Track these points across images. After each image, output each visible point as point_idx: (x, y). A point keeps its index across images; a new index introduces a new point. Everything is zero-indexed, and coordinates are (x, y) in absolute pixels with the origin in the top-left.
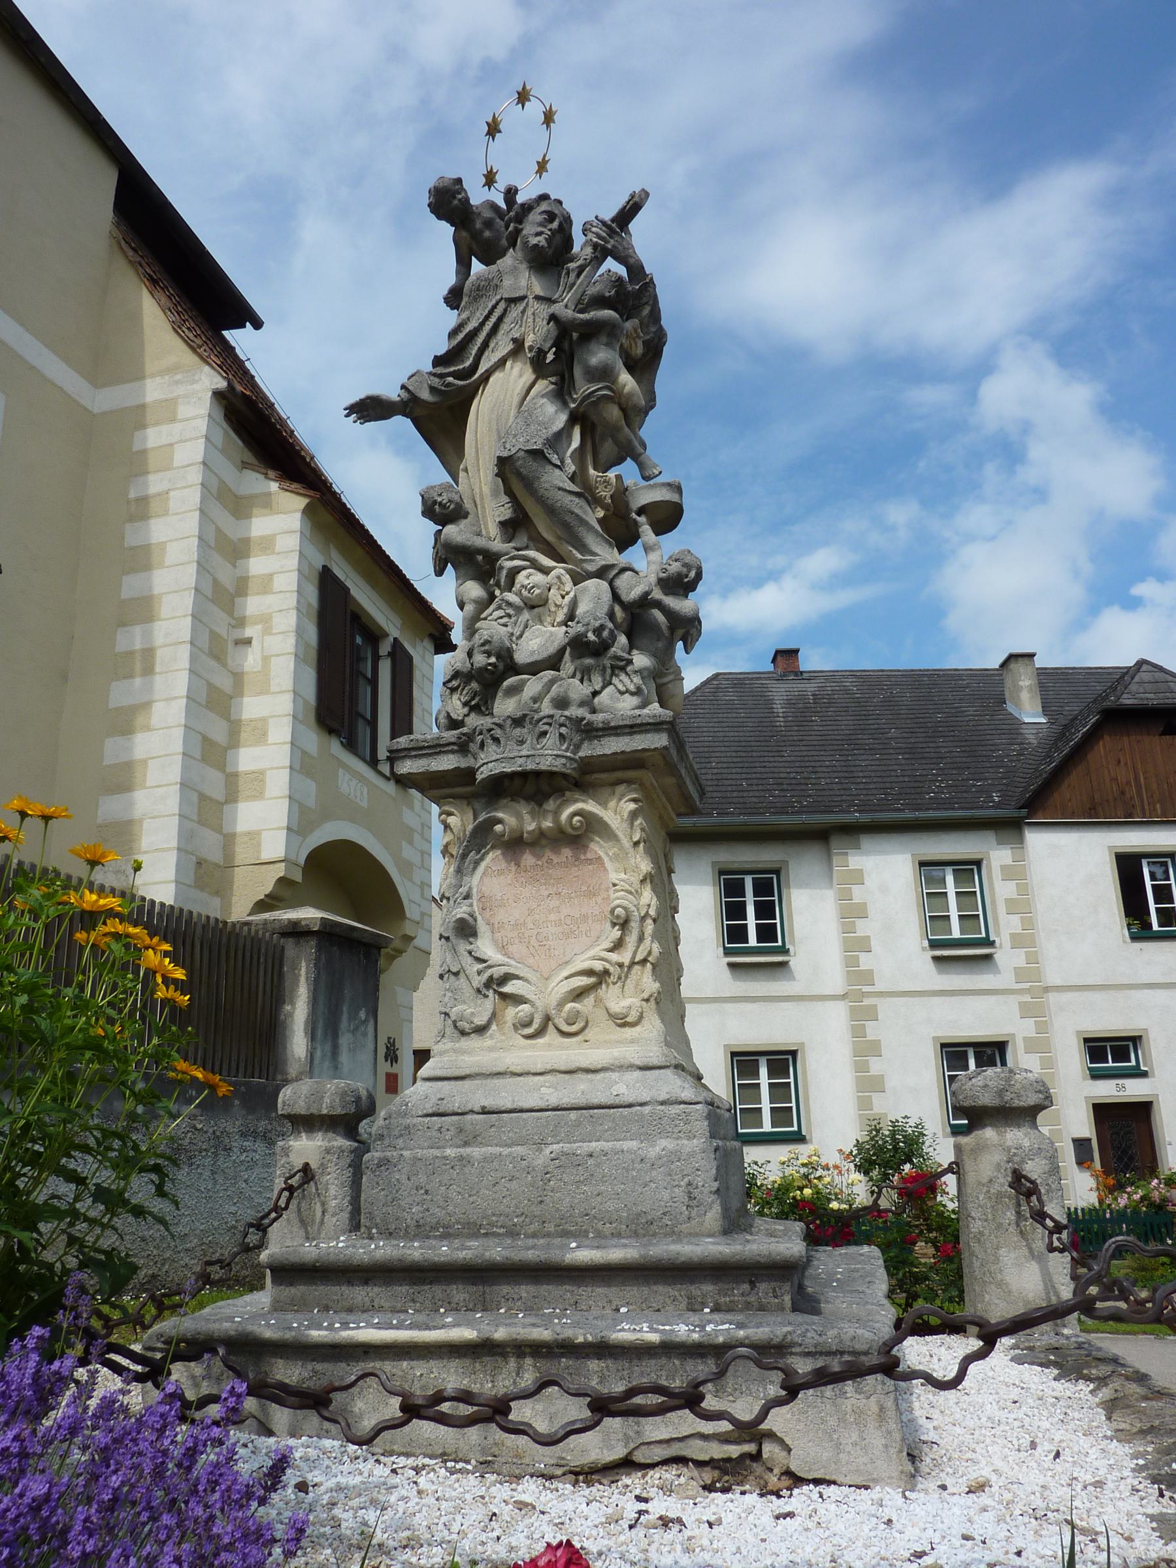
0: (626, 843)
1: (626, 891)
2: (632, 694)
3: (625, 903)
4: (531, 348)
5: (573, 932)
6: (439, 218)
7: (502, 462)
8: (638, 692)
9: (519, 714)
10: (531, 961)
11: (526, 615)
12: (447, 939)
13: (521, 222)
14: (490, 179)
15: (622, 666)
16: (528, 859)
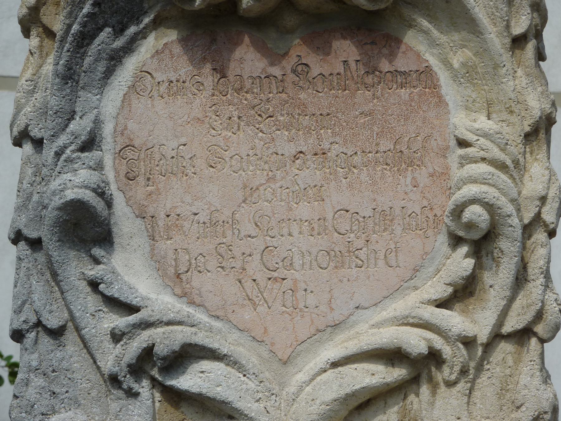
0: (496, 41)
1: (493, 163)
3: (491, 194)
5: (353, 252)
6: (19, 23)
10: (247, 315)
12: (36, 244)
16: (247, 59)
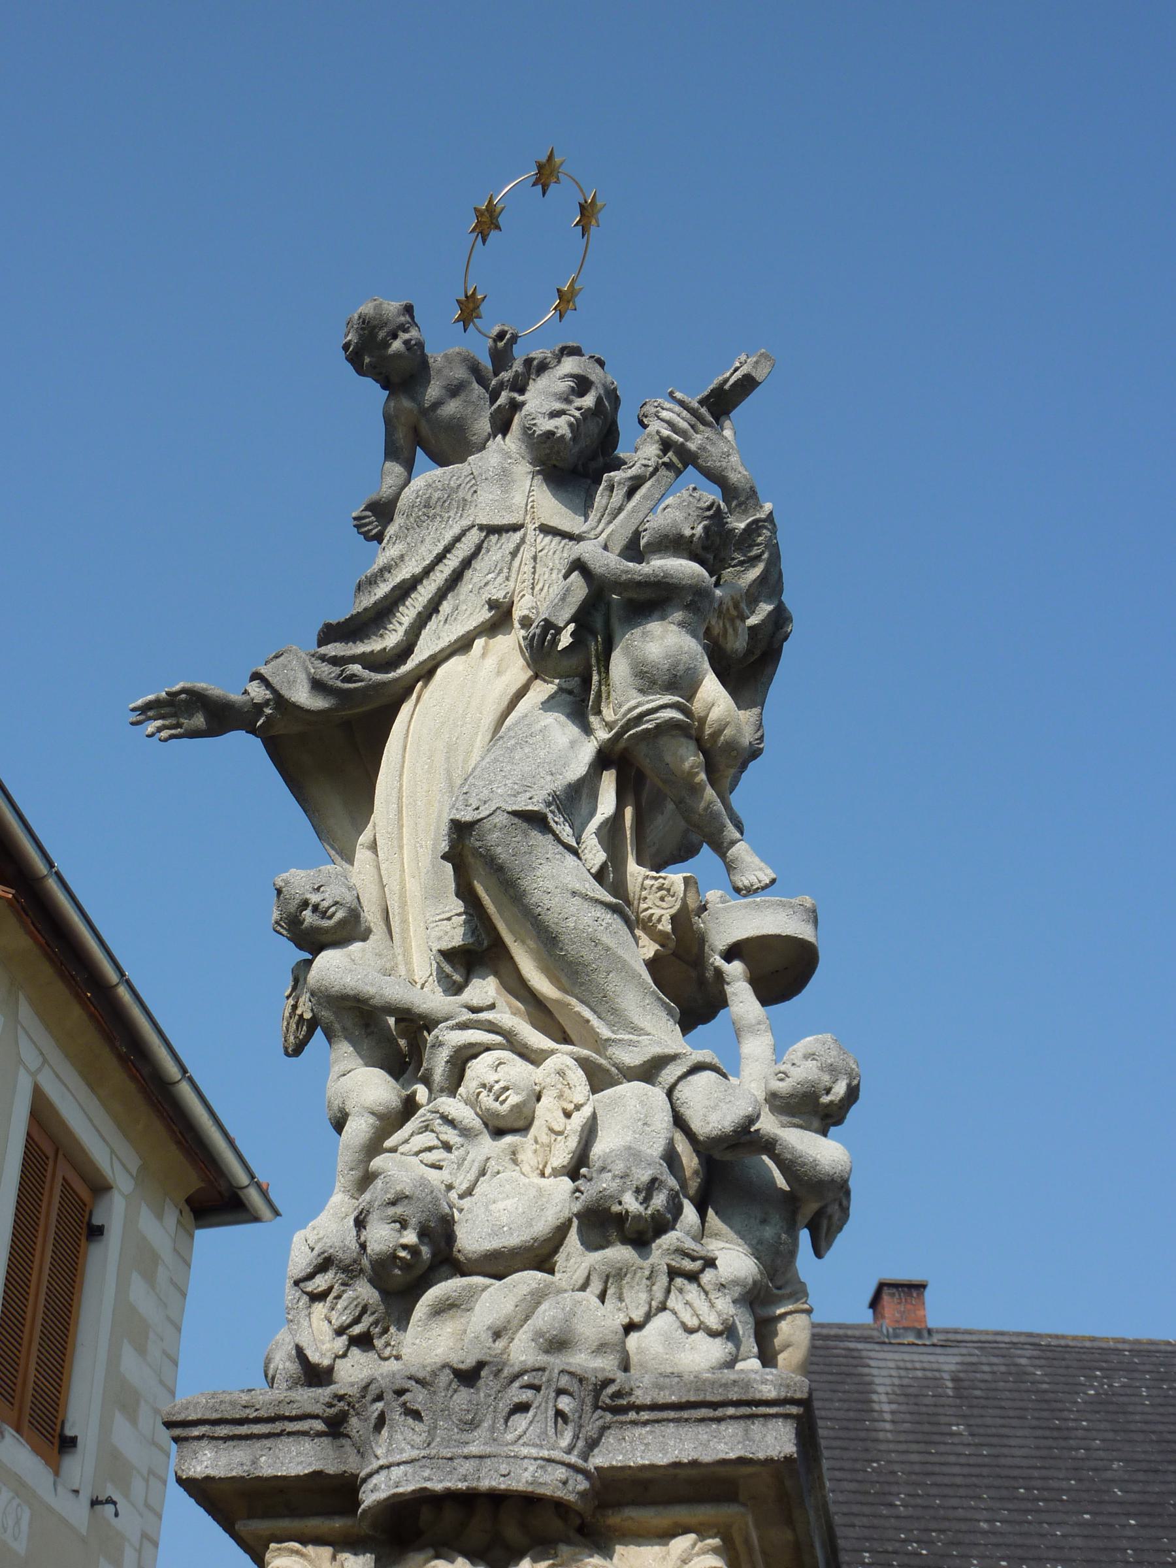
2: (713, 1334)
4: (526, 622)
7: (461, 830)
8: (728, 1332)
9: (469, 1362)
11: (487, 1146)
13: (522, 391)
14: (469, 310)
15: (691, 1271)
